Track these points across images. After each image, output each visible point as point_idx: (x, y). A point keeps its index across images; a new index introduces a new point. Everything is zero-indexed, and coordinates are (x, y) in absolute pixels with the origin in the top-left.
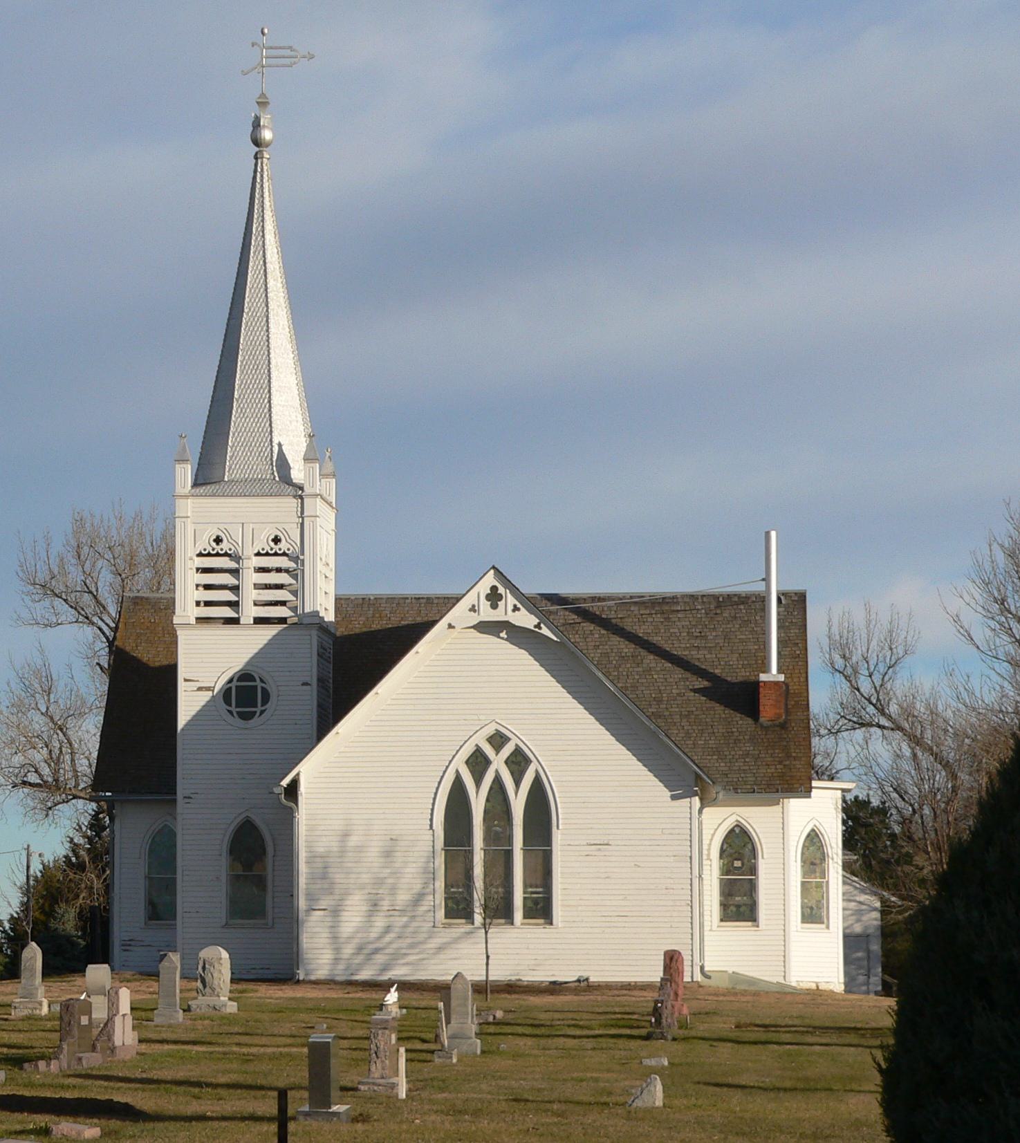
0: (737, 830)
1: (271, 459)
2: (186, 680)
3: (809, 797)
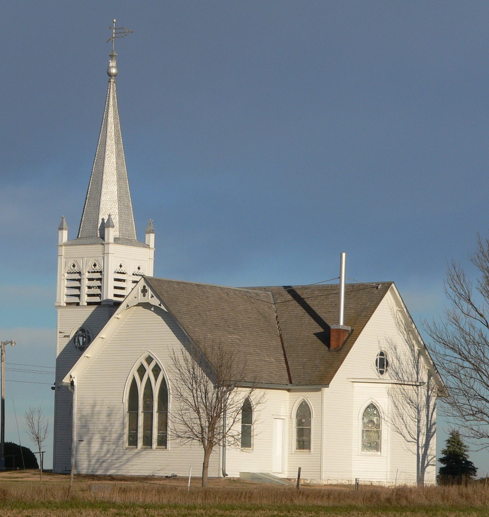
0: (304, 404)
2: (60, 332)
3: (328, 387)
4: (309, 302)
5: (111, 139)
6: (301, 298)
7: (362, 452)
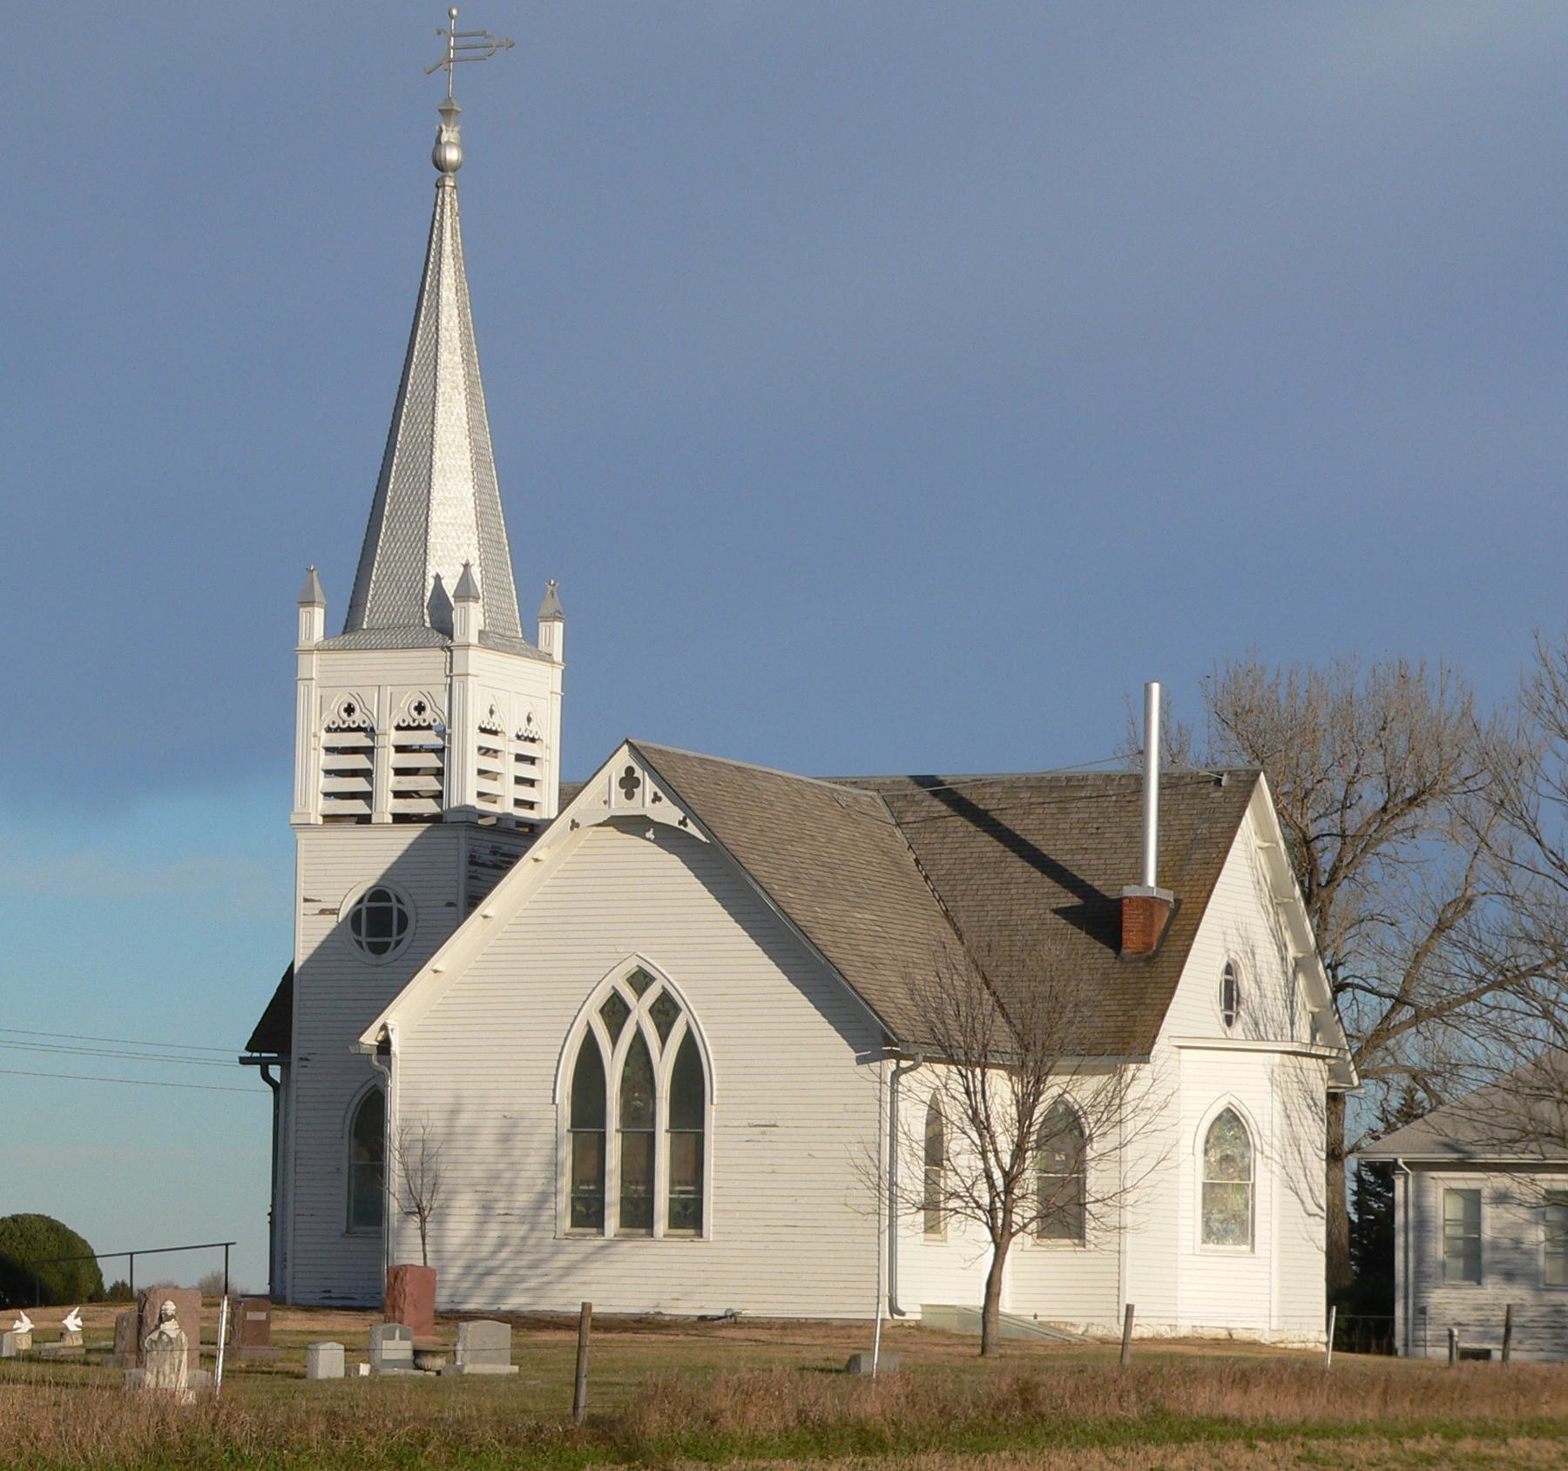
1: (422, 599)
2: (306, 900)
4: (1007, 821)
5: (452, 349)
6: (980, 810)
7: (1205, 1246)
